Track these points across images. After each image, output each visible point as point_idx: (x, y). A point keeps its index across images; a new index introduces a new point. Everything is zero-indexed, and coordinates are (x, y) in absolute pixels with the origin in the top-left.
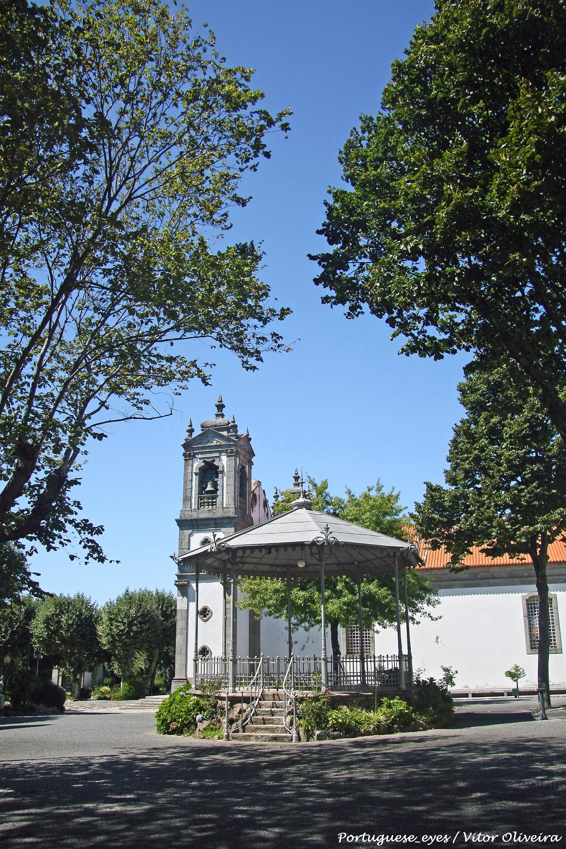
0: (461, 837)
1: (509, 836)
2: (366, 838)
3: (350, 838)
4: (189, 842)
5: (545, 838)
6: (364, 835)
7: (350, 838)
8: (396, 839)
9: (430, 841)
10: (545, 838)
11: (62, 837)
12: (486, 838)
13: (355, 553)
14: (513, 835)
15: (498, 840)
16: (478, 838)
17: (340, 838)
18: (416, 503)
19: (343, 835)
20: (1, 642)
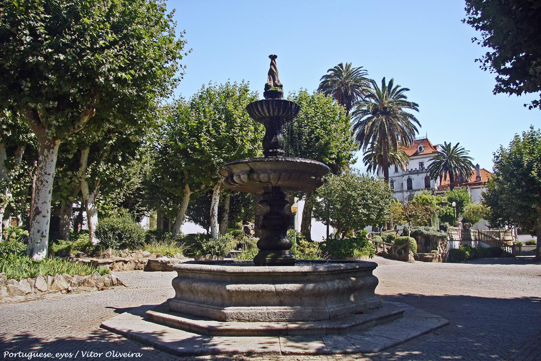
0: (80, 354)
1: (109, 353)
2: (21, 355)
3: (11, 355)
4: (35, 346)
5: (132, 355)
6: (20, 353)
7: (11, 355)
8: (40, 355)
9: (61, 356)
10: (132, 355)
11: (19, 340)
12: (96, 355)
13: (254, 302)
14: (112, 353)
15: (103, 356)
16: (92, 355)
17: (5, 355)
18: (498, 90)
19: (7, 353)
20: (52, 1)
